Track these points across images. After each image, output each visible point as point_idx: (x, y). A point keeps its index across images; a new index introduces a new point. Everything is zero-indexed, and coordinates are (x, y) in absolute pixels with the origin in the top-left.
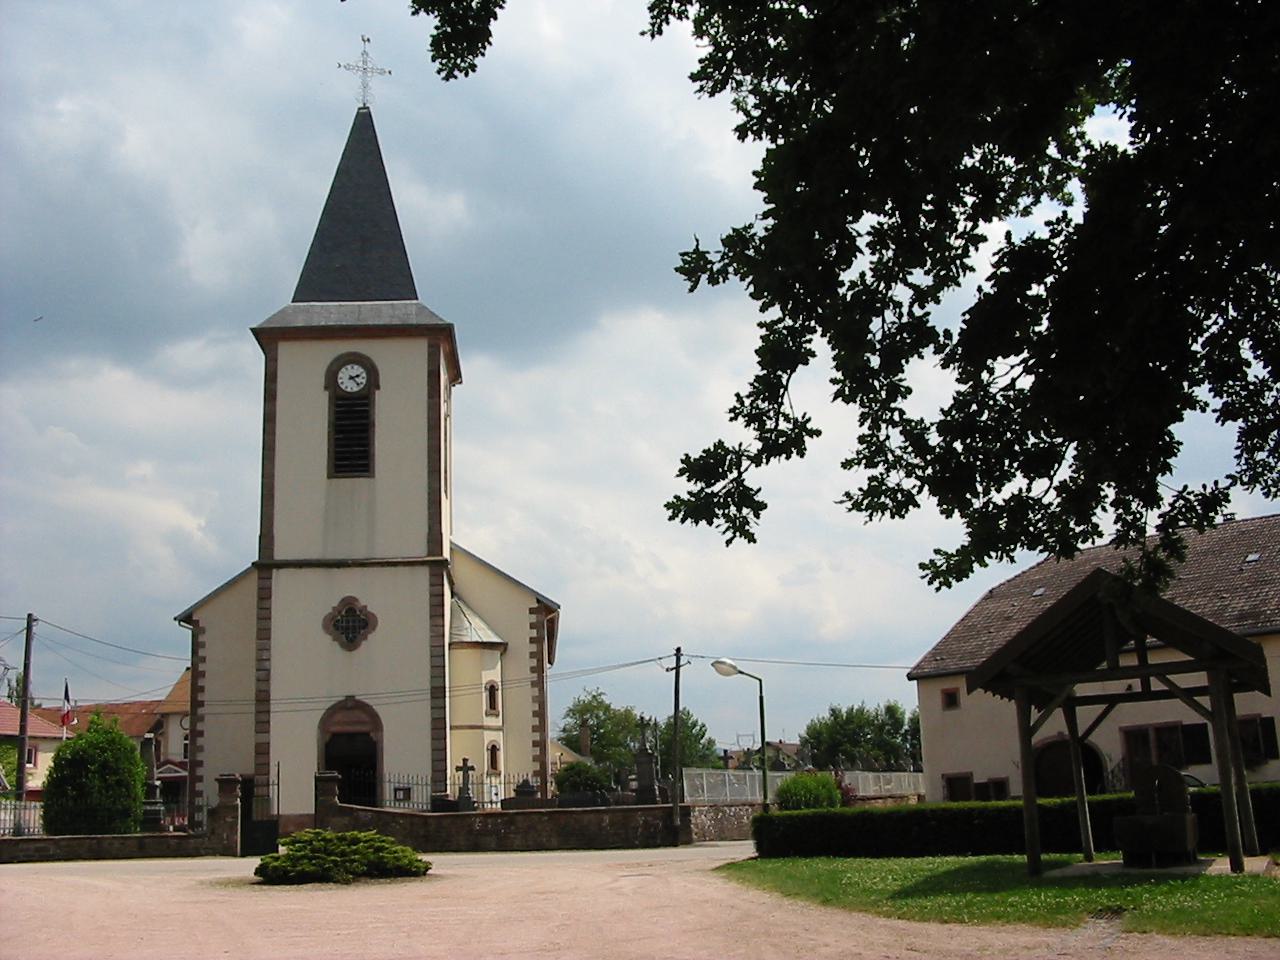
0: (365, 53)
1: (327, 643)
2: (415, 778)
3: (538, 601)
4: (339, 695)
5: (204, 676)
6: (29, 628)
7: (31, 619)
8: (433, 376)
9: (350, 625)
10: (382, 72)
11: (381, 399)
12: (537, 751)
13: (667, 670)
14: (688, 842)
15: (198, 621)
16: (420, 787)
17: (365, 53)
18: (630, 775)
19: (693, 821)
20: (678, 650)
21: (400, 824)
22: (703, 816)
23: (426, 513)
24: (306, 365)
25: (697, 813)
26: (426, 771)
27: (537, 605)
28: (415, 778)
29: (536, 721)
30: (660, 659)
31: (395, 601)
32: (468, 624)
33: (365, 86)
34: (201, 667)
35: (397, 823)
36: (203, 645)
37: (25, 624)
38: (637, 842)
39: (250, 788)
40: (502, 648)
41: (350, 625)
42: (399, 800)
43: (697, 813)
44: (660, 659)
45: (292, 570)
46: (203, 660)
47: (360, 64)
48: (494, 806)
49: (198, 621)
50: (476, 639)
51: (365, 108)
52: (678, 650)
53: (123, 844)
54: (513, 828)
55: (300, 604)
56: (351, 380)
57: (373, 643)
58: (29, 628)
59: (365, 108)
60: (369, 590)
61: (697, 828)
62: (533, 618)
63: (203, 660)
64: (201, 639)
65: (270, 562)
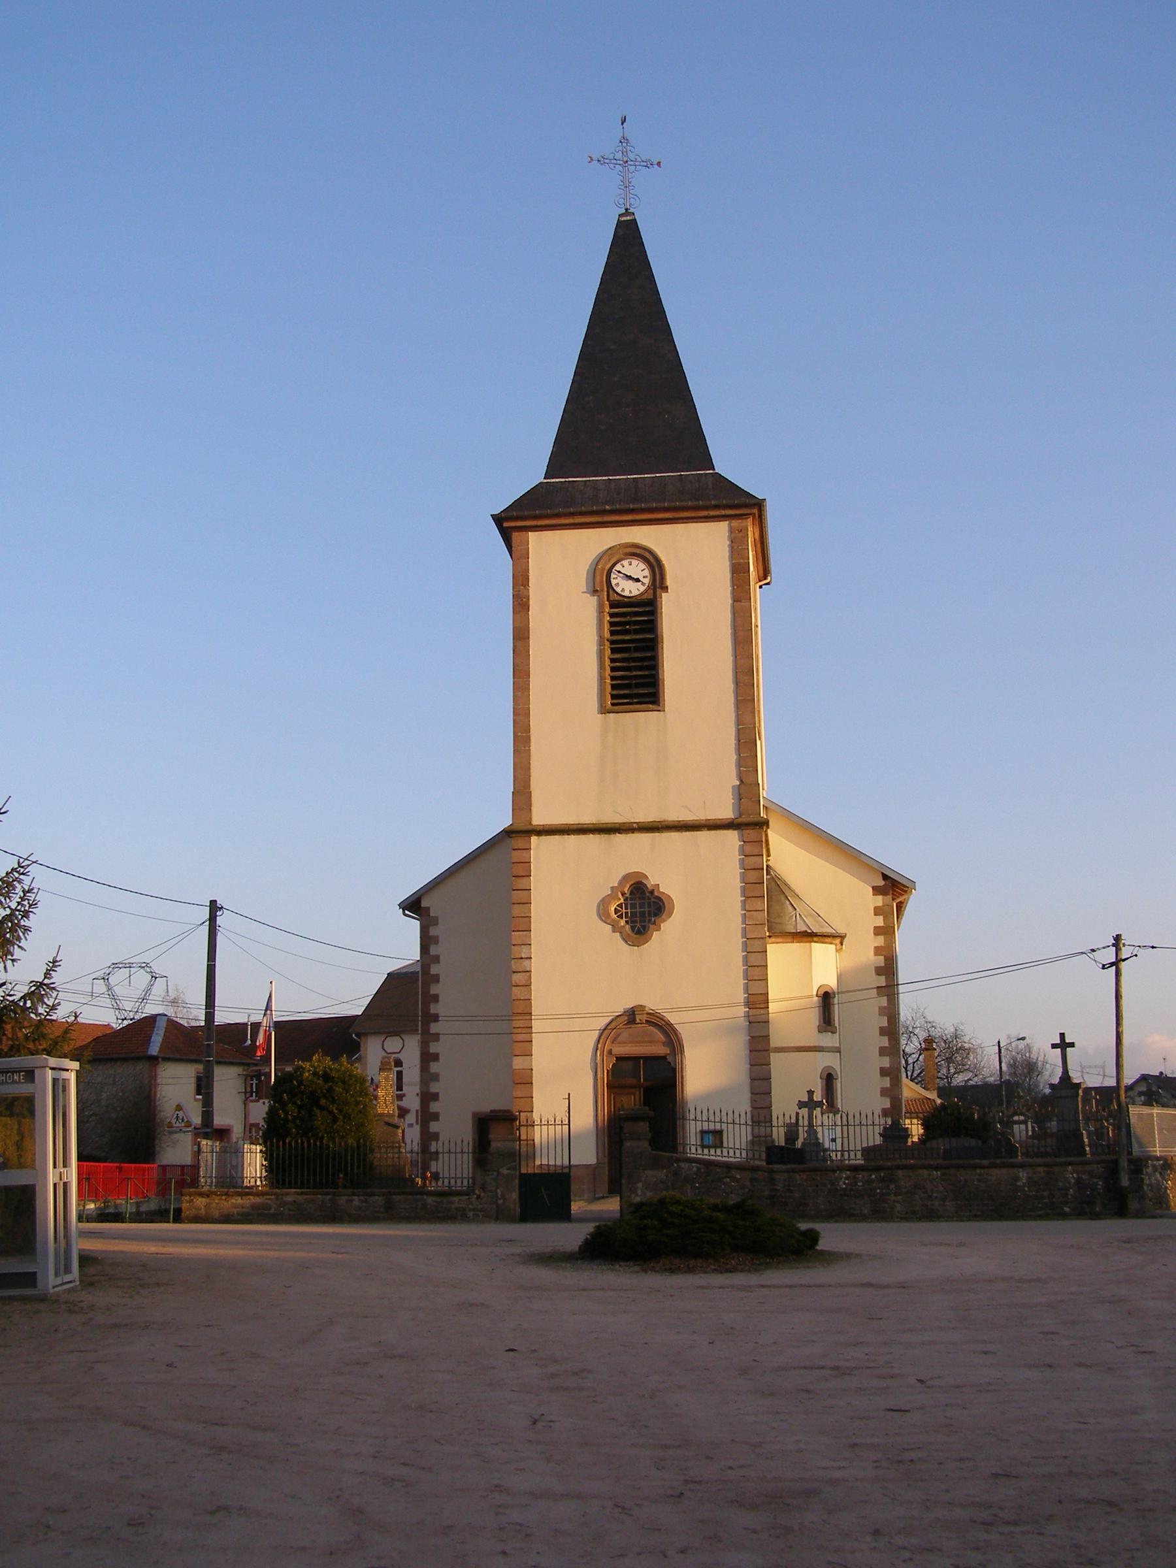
0: (624, 140)
1: (607, 941)
2: (718, 1113)
3: (885, 877)
4: (620, 1006)
5: (438, 981)
6: (213, 919)
7: (214, 907)
8: (739, 571)
9: (641, 909)
10: (648, 164)
11: (667, 603)
12: (886, 1082)
13: (1104, 967)
14: (1140, 1214)
15: (428, 909)
16: (453, 1156)
17: (624, 140)
18: (1016, 1114)
19: (1147, 1182)
20: (1118, 938)
21: (737, 1180)
22: (1158, 1175)
23: (734, 758)
24: (565, 557)
25: (1150, 1170)
26: (743, 1105)
27: (883, 883)
28: (718, 1113)
29: (885, 1041)
30: (1093, 950)
31: (700, 879)
32: (790, 908)
33: (626, 186)
34: (434, 970)
35: (733, 1179)
36: (435, 940)
37: (205, 913)
38: (1067, 1209)
39: (497, 1127)
40: (838, 941)
41: (641, 909)
42: (709, 1147)
43: (1150, 1170)
44: (1093, 950)
45: (557, 837)
46: (437, 959)
47: (619, 155)
48: (440, 1183)
49: (428, 909)
50: (801, 928)
51: (627, 212)
52: (1118, 938)
53: (366, 1201)
54: (892, 1186)
55: (565, 889)
56: (631, 581)
57: (668, 932)
58: (213, 919)
59: (627, 212)
60: (664, 864)
61: (1151, 1190)
62: (879, 900)
63: (437, 959)
64: (433, 932)
65: (529, 827)
